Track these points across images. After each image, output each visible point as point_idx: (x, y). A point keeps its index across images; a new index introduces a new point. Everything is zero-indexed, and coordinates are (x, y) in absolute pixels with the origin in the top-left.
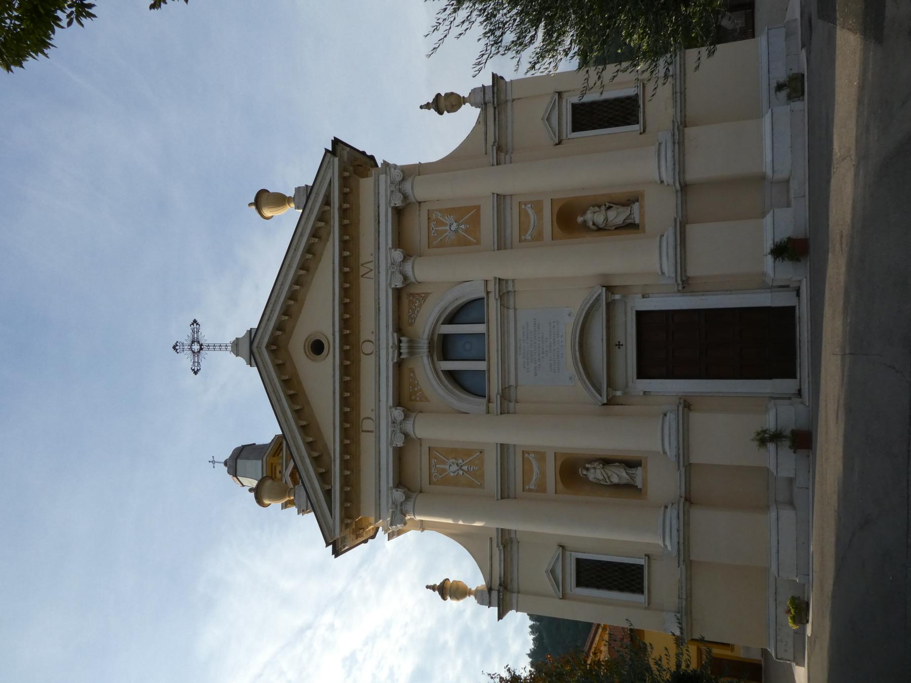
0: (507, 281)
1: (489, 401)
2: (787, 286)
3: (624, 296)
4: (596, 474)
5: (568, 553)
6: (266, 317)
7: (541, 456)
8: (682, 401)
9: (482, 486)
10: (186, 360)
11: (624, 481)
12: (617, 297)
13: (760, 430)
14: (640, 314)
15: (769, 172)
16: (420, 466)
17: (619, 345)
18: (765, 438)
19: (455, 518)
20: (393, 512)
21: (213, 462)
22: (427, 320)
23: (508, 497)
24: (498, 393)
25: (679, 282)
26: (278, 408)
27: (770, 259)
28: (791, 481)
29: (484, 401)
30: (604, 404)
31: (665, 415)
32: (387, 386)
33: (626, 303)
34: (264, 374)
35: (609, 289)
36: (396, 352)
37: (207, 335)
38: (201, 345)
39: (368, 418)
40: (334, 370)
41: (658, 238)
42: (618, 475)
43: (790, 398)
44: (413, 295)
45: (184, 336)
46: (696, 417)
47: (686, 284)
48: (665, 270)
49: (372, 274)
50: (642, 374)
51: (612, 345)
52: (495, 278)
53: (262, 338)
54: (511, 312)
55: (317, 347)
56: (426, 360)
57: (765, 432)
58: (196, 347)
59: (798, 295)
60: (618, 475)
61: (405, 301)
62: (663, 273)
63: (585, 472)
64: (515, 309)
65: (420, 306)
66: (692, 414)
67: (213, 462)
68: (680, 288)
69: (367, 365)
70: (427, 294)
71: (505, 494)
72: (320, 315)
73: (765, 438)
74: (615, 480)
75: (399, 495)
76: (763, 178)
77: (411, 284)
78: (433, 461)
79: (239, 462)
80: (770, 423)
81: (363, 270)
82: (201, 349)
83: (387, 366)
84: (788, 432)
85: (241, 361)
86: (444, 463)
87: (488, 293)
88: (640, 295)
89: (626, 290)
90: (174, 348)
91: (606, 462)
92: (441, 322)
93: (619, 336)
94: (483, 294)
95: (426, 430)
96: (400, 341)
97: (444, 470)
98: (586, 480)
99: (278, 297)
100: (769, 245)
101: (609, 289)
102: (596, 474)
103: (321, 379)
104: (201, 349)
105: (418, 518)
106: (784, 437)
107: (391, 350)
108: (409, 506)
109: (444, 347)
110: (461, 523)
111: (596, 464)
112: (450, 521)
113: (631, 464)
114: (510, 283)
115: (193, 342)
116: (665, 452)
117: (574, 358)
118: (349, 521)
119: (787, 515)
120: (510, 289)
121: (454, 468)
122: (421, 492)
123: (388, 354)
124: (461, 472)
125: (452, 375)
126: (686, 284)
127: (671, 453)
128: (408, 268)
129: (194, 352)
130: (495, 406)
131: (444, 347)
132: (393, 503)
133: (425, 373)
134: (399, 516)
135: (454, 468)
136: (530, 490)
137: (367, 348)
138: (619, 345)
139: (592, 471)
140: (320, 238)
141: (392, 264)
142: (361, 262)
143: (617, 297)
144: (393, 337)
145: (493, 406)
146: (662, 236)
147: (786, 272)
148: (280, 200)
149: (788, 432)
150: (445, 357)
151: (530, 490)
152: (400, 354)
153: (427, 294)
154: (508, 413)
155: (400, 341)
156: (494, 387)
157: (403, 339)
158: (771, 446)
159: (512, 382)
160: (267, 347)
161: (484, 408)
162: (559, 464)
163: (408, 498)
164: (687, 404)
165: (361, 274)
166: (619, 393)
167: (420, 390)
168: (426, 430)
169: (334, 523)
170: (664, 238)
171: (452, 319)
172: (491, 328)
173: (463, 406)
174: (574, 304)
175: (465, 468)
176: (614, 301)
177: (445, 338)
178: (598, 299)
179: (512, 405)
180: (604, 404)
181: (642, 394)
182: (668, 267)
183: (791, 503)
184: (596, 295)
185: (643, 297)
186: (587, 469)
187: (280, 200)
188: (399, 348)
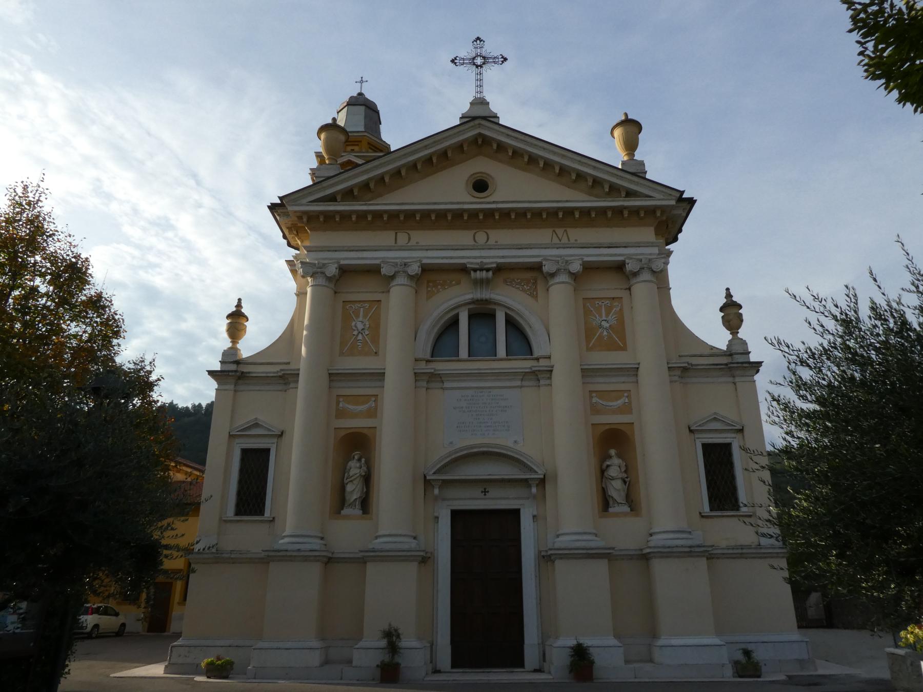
0: (550, 378)
1: (428, 361)
2: (544, 660)
3: (535, 497)
4: (355, 468)
5: (275, 440)
6: (510, 133)
7: (373, 413)
8: (429, 555)
9: (342, 354)
10: (466, 51)
11: (347, 497)
12: (534, 490)
13: (400, 632)
14: (516, 513)
15: (661, 642)
16: (362, 291)
17: (485, 492)
18: (392, 637)
19: (309, 327)
20: (315, 264)
21: (362, 82)
22: (509, 297)
23: (331, 381)
24: (435, 370)
25: (550, 552)
26: (418, 146)
27: (572, 642)
28: (349, 662)
29: (428, 357)
30: (425, 477)
31: (415, 538)
32: (443, 258)
33: (528, 498)
34: (450, 133)
35: (542, 482)
36: (477, 266)
37: (491, 73)
38: (481, 66)
39: (409, 239)
40: (458, 203)
41: (594, 531)
42: (354, 490)
43: (431, 662)
44: (535, 283)
45: (491, 48)
46: (412, 568)
47: (546, 559)
48: (561, 538)
49: (556, 240)
50: (456, 515)
51: (485, 485)
52: (553, 367)
53: (489, 129)
54: (518, 383)
55: (480, 186)
56: (469, 297)
57: (398, 636)
58: (479, 61)
59: (536, 671)
60: (354, 490)
61: (529, 275)
62: (558, 536)
63: (356, 457)
64: (521, 387)
65: (523, 290)
66: (415, 564)
67: (362, 82)
68: (543, 554)
69: (463, 237)
70: (535, 297)
71: (334, 377)
72: (513, 188)
73: (392, 637)
74: (349, 488)
75: (332, 270)
76: (655, 635)
77: (547, 282)
78: (367, 305)
79: (363, 108)
80: (408, 642)
81: (560, 231)
82: (477, 66)
83: (463, 258)
84: (397, 659)
85: (465, 108)
86: (365, 316)
87: (537, 359)
88: (535, 513)
89: (542, 498)
90: (478, 38)
91: (367, 479)
92: (508, 312)
93: (493, 492)
94: (536, 355)
95: (398, 297)
96: (488, 270)
97: (358, 316)
98: (348, 458)
99: (531, 145)
100: (587, 642)
101: (542, 482)
102: (355, 468)
103: (448, 190)
104: (477, 66)
105: (309, 290)
106: (393, 655)
107: (479, 261)
108: (321, 281)
109: (482, 315)
110: (305, 333)
111: (364, 468)
112: (306, 322)
113: (365, 504)
114: (548, 382)
115: (484, 58)
116: (377, 538)
117: (472, 447)
118: (305, 220)
119: (315, 659)
120: (542, 382)
121: (360, 326)
122: (336, 293)
123: (475, 258)
124: (355, 333)
125: (454, 323)
126: (546, 559)
127: (377, 544)
128: (563, 278)
129: (474, 58)
130: (423, 367)
131: (482, 315)
132: (324, 265)
133: (456, 296)
134: (311, 271)
135: (360, 326)
136: (338, 403)
137: (481, 237)
138: (485, 492)
139: (358, 465)
140: (593, 186)
141: (567, 262)
142: (568, 230)
143: (534, 490)
144: (492, 263)
145: (423, 365)
146: (596, 535)
147: (559, 658)
148: (631, 145)
149: (397, 659)
150: (471, 317)
151: (338, 403)
152: (475, 270)
153: (535, 297)
154: (416, 381)
155: (488, 270)
156: (442, 367)
157: (490, 273)
158: (383, 643)
159: (447, 385)
160: (480, 134)
161: (421, 356)
162: (365, 431)
163: (329, 279)
164: (426, 560)
165: (558, 231)
166: (436, 491)
167: (438, 291)
168: (398, 297)
169: (302, 205)
170: (594, 538)
171: (511, 323)
172: (502, 361)
173: (422, 335)
174: (528, 447)
175: (360, 337)
176: (530, 486)
177: (492, 316)
178: (531, 470)
179: (424, 384)
180: (425, 477)
181: (436, 514)
182: (564, 541)
183: (326, 662)
184: (535, 468)
185: (534, 517)
186: (359, 460)
187: (631, 145)
188: (481, 270)
